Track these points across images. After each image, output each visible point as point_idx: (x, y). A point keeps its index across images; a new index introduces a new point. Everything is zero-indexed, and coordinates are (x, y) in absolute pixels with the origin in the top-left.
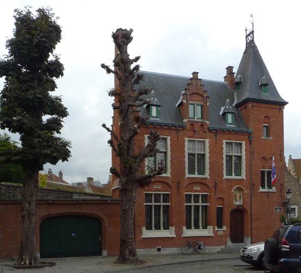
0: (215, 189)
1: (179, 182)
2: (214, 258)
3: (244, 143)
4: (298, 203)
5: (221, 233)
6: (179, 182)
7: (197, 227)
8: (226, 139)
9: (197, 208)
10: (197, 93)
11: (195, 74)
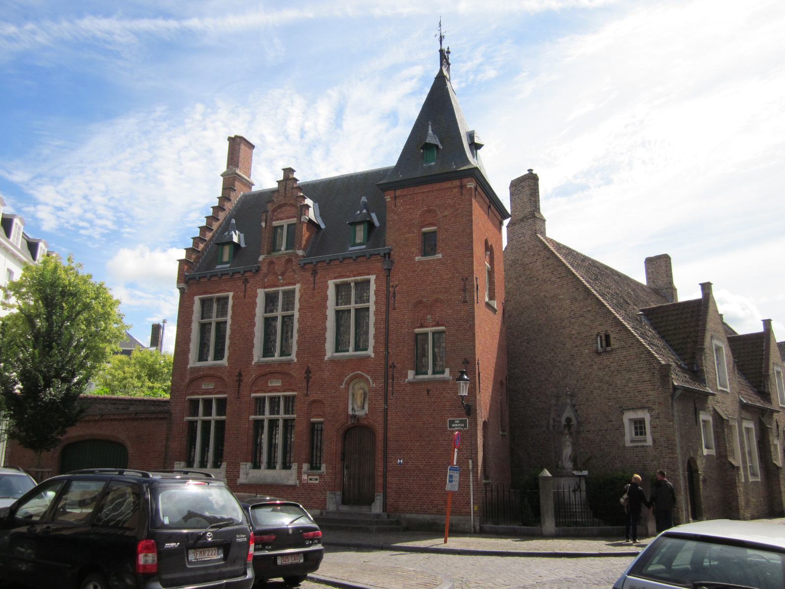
0: (308, 382)
1: (240, 375)
2: (398, 556)
3: (372, 278)
4: (650, 405)
5: (315, 480)
6: (240, 375)
7: (271, 465)
8: (335, 278)
9: (273, 423)
10: (285, 205)
11: (218, 198)
